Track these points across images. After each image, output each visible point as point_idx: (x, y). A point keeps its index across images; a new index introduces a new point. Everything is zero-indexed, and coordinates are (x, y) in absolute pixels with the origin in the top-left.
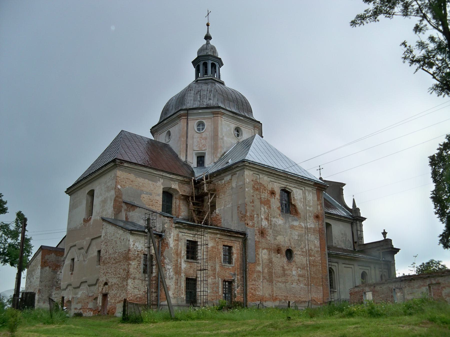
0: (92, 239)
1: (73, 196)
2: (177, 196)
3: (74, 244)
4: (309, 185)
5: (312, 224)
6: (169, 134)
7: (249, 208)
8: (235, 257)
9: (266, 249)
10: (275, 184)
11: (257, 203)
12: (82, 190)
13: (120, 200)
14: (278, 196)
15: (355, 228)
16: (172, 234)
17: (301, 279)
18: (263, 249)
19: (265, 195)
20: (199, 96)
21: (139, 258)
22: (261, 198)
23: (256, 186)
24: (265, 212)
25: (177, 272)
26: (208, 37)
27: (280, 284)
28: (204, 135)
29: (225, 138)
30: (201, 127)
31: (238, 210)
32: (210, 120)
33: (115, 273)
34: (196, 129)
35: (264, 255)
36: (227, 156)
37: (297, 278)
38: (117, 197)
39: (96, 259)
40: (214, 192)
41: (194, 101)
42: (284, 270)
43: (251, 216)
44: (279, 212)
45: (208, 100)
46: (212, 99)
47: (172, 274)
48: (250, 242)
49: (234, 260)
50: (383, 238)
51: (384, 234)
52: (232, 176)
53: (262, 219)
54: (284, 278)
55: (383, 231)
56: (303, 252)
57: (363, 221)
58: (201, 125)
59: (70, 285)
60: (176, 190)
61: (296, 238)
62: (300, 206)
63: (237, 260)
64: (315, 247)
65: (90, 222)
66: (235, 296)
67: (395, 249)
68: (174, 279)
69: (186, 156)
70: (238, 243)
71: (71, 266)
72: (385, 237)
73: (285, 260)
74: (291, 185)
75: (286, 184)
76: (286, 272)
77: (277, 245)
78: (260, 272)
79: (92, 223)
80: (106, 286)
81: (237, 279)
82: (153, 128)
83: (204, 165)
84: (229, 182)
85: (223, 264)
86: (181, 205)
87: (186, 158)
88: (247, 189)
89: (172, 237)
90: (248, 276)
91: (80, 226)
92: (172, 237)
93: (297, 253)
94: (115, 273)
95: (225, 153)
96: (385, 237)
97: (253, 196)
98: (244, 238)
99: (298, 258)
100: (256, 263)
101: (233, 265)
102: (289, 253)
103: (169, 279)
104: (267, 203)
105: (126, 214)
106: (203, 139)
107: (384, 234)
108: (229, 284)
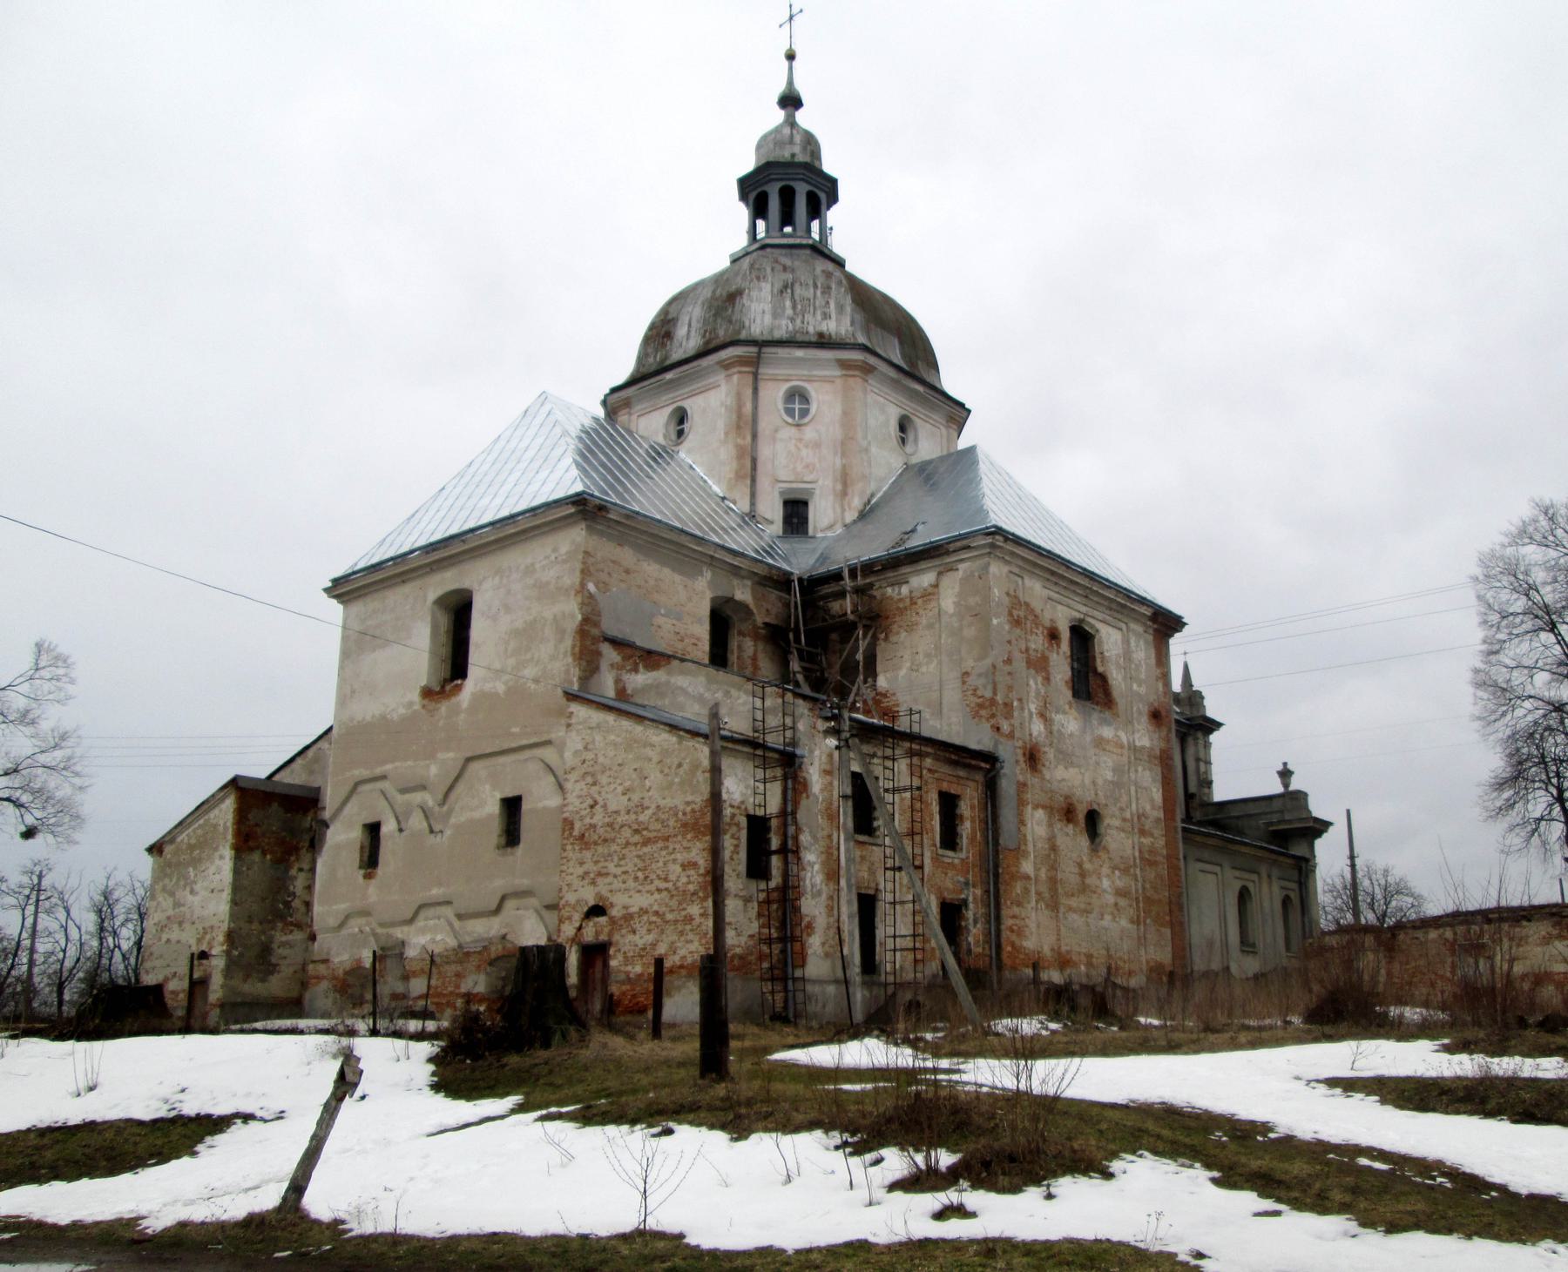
0: (469, 760)
1: (358, 607)
2: (746, 627)
3: (378, 771)
4: (1137, 617)
5: (1144, 737)
6: (681, 417)
7: (1002, 679)
8: (966, 829)
9: (1044, 807)
10: (1060, 607)
11: (1019, 664)
12: (407, 589)
13: (595, 632)
14: (1065, 646)
15: (1191, 751)
16: (817, 753)
17: (1123, 902)
18: (1036, 807)
19: (1038, 642)
20: (788, 303)
21: (734, 829)
22: (1027, 650)
23: (1015, 613)
24: (1038, 693)
25: (832, 875)
26: (790, 101)
27: (1075, 916)
28: (809, 433)
29: (873, 449)
30: (797, 406)
31: (964, 683)
32: (827, 386)
33: (640, 874)
34: (781, 406)
35: (1037, 825)
36: (877, 504)
37: (1110, 899)
38: (586, 620)
39: (496, 827)
40: (876, 620)
41: (775, 315)
42: (1083, 874)
43: (1006, 704)
44: (1069, 694)
45: (819, 317)
46: (834, 316)
47: (819, 879)
48: (1006, 786)
49: (964, 841)
50: (1279, 789)
51: (1285, 774)
52: (940, 574)
53: (1031, 714)
54: (1082, 898)
55: (1280, 767)
56: (1124, 820)
57: (1211, 731)
58: (797, 398)
59: (365, 913)
60: (747, 607)
61: (1109, 775)
62: (1116, 678)
63: (972, 839)
64: (1153, 808)
65: (454, 700)
66: (969, 951)
67: (1316, 820)
68: (824, 896)
69: (753, 495)
70: (971, 784)
71: (362, 848)
72: (1286, 785)
73: (1084, 841)
74: (1096, 613)
75: (1084, 609)
76: (1088, 881)
77: (1067, 797)
78: (1027, 878)
79: (465, 705)
80: (602, 920)
81: (973, 895)
82: (614, 390)
83: (806, 532)
84: (931, 593)
85: (941, 851)
86: (761, 656)
87: (753, 504)
88: (995, 622)
89: (816, 763)
90: (1002, 888)
91: (402, 711)
92: (816, 763)
93: (1111, 823)
94: (640, 874)
95: (873, 495)
96: (1286, 785)
97: (1009, 642)
98: (989, 771)
99: (1117, 839)
100: (1019, 852)
101: (963, 855)
102: (1092, 821)
103: (813, 897)
104: (1039, 665)
105: (617, 681)
106: (807, 447)
107: (1285, 774)
108: (951, 914)
